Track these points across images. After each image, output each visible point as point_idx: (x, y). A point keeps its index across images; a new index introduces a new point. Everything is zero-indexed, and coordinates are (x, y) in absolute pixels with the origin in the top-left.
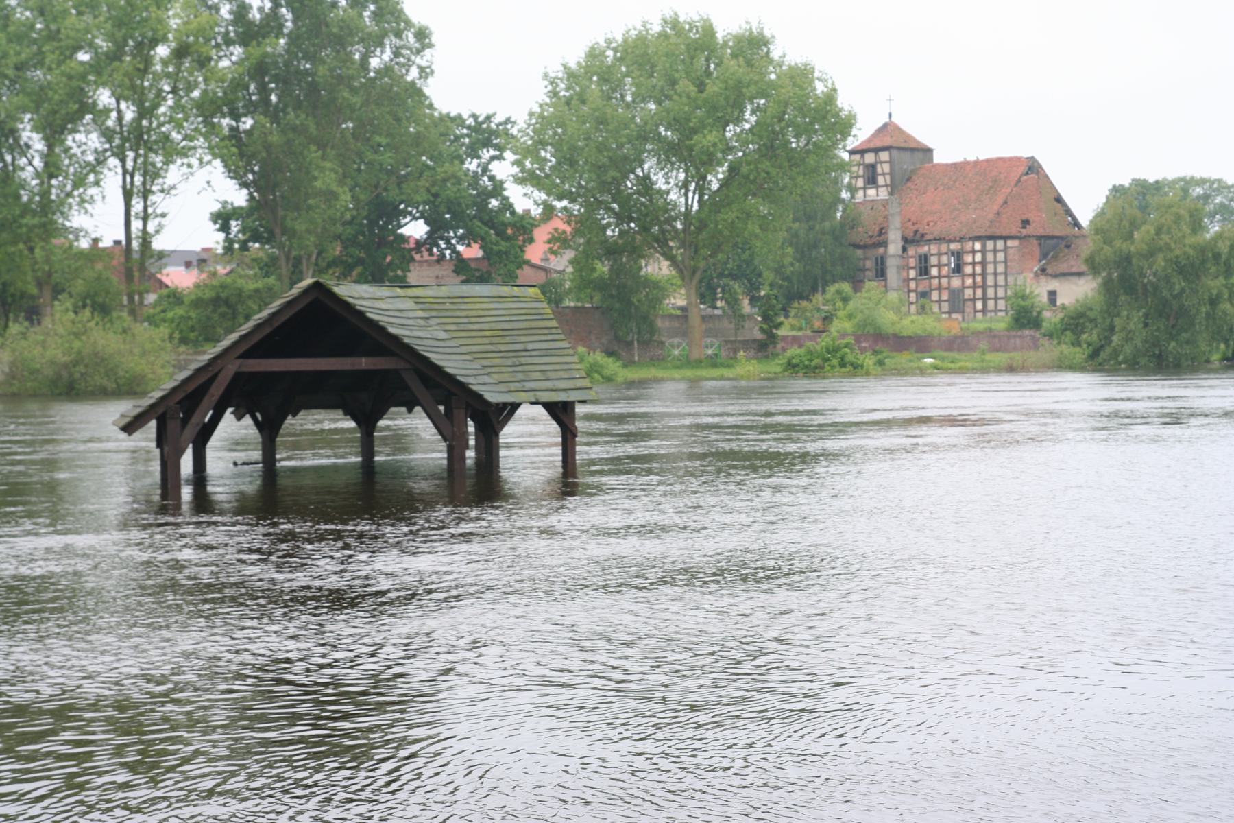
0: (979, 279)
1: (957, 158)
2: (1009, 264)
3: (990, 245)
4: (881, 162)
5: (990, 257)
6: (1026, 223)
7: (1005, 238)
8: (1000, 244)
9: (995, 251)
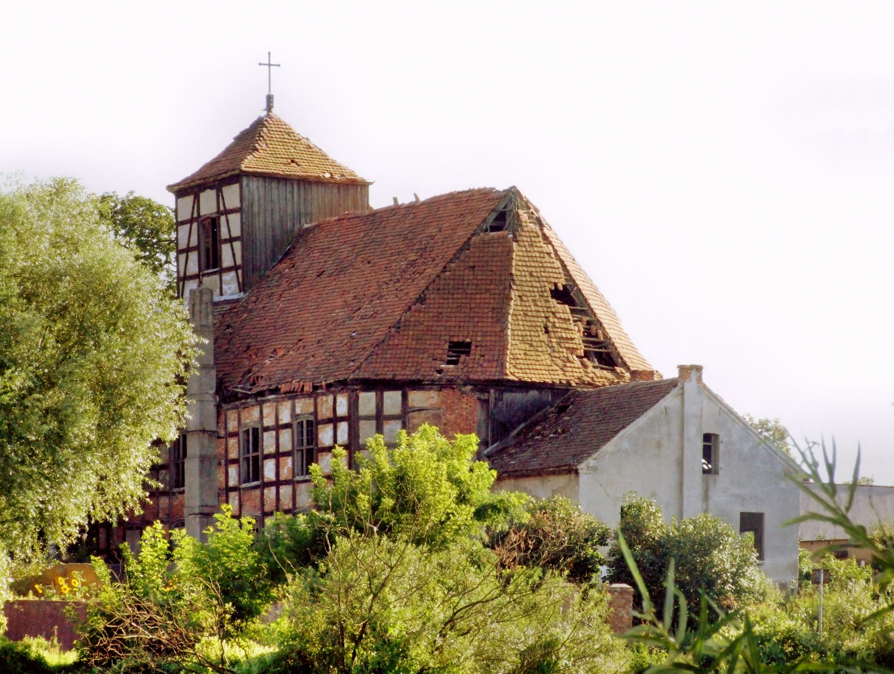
3: (367, 401)
6: (460, 349)
7: (405, 386)
8: (392, 400)
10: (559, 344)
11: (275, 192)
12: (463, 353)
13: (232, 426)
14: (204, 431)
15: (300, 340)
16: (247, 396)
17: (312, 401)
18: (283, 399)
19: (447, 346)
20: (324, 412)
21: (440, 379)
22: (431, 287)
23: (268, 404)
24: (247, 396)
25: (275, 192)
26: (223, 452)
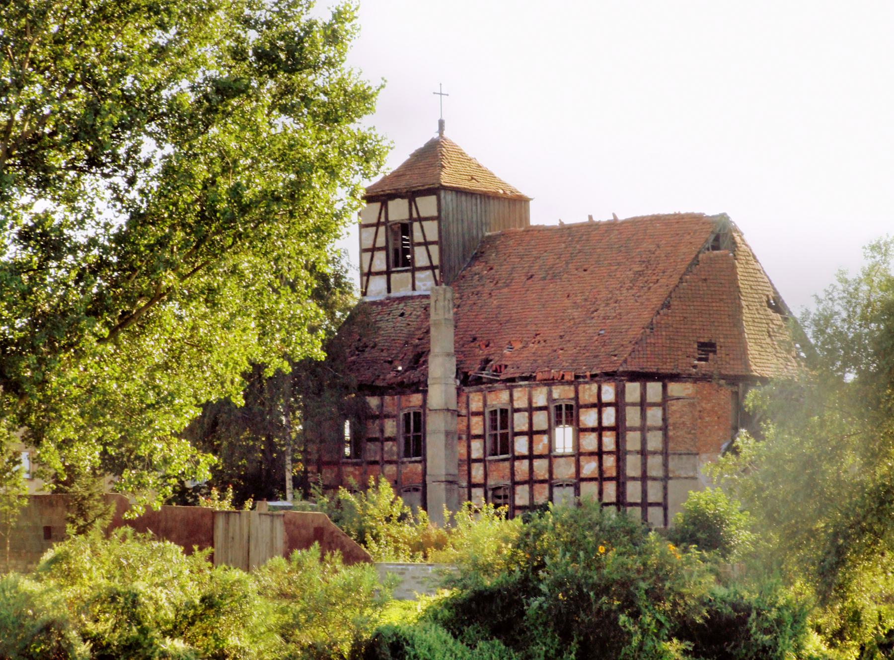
0: (609, 462)
1: (575, 217)
2: (671, 433)
3: (633, 390)
4: (420, 219)
5: (633, 417)
6: (707, 348)
7: (665, 378)
8: (654, 390)
9: (643, 404)
10: (779, 346)
11: (464, 203)
12: (711, 351)
13: (476, 404)
14: (448, 410)
15: (536, 335)
16: (491, 381)
17: (572, 388)
18: (537, 385)
19: (696, 346)
20: (587, 397)
21: (697, 373)
22: (673, 295)
23: (520, 389)
24: (491, 381)
25: (464, 203)
26: (465, 428)
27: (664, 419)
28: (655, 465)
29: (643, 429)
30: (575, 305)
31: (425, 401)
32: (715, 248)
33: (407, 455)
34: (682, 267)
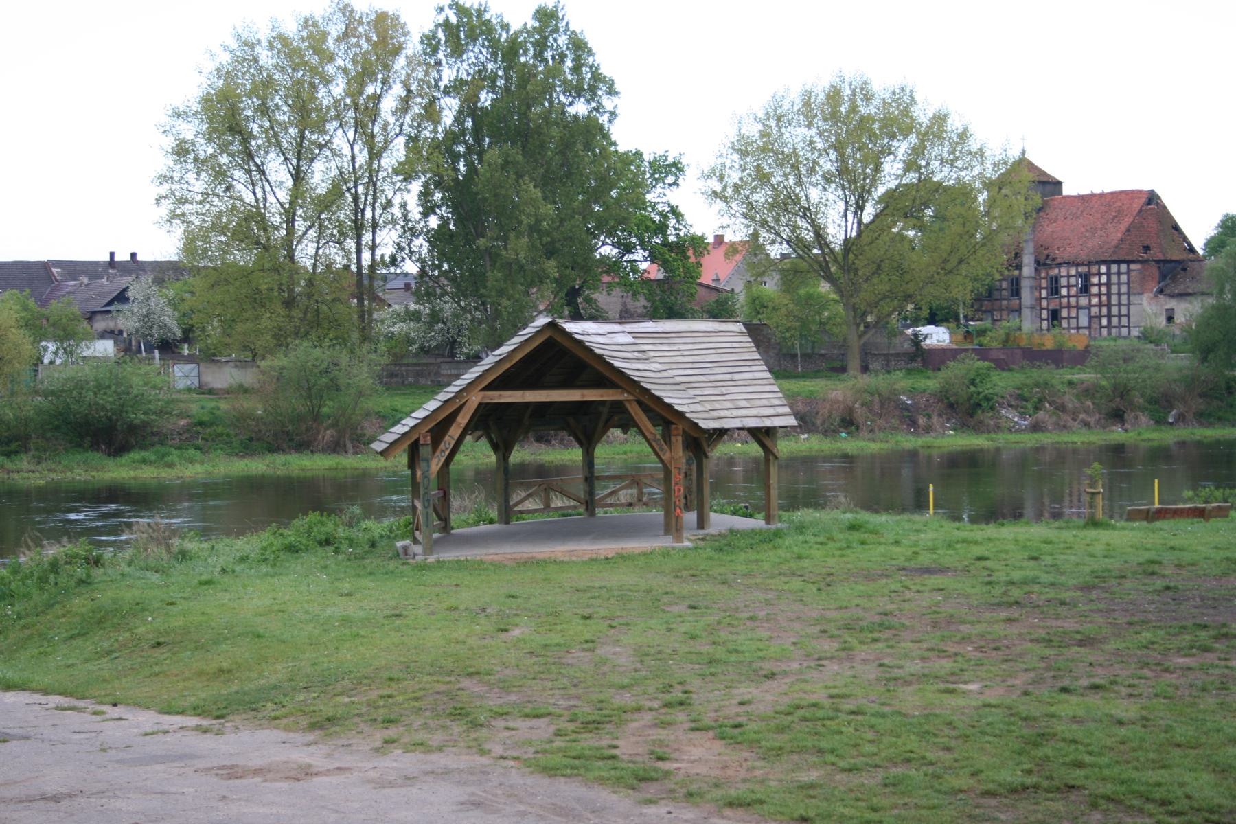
0: (1104, 298)
1: (1085, 191)
3: (1114, 268)
5: (1114, 279)
7: (1128, 262)
8: (1124, 267)
9: (1119, 273)
27: (1128, 280)
28: (1124, 299)
29: (1119, 284)
30: (1087, 231)
31: (1020, 274)
32: (1149, 204)
33: (1012, 296)
34: (1135, 213)
